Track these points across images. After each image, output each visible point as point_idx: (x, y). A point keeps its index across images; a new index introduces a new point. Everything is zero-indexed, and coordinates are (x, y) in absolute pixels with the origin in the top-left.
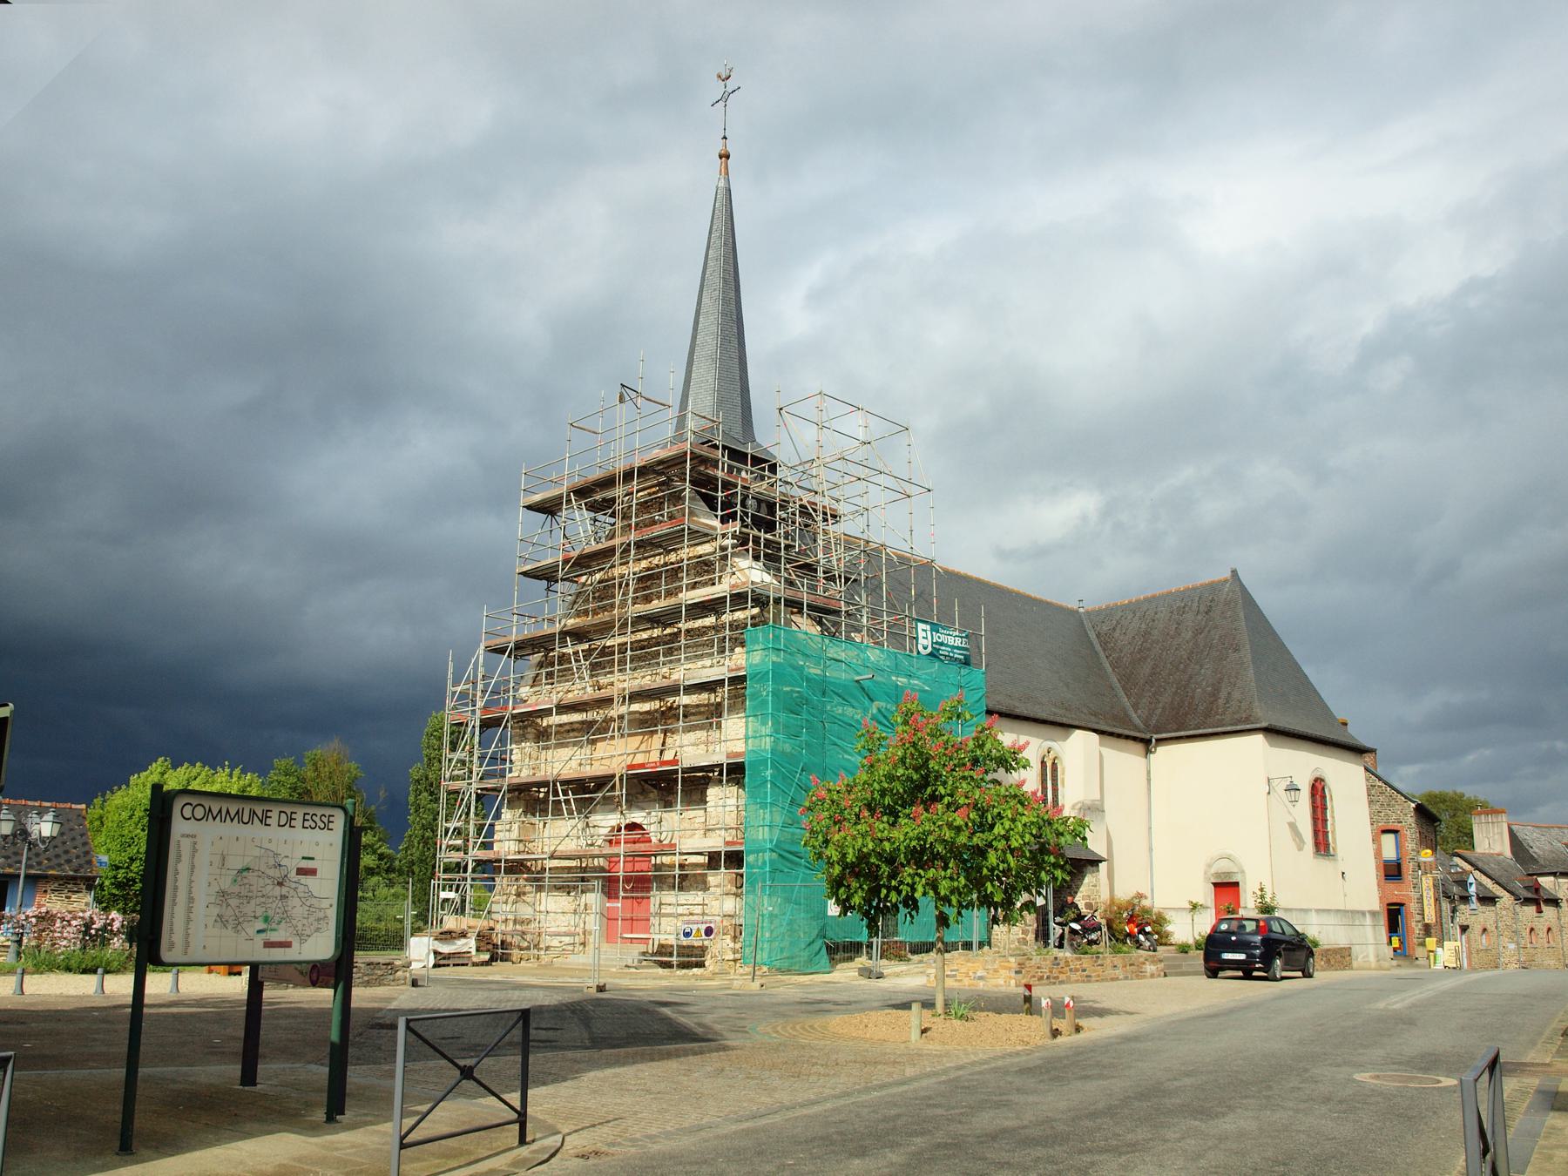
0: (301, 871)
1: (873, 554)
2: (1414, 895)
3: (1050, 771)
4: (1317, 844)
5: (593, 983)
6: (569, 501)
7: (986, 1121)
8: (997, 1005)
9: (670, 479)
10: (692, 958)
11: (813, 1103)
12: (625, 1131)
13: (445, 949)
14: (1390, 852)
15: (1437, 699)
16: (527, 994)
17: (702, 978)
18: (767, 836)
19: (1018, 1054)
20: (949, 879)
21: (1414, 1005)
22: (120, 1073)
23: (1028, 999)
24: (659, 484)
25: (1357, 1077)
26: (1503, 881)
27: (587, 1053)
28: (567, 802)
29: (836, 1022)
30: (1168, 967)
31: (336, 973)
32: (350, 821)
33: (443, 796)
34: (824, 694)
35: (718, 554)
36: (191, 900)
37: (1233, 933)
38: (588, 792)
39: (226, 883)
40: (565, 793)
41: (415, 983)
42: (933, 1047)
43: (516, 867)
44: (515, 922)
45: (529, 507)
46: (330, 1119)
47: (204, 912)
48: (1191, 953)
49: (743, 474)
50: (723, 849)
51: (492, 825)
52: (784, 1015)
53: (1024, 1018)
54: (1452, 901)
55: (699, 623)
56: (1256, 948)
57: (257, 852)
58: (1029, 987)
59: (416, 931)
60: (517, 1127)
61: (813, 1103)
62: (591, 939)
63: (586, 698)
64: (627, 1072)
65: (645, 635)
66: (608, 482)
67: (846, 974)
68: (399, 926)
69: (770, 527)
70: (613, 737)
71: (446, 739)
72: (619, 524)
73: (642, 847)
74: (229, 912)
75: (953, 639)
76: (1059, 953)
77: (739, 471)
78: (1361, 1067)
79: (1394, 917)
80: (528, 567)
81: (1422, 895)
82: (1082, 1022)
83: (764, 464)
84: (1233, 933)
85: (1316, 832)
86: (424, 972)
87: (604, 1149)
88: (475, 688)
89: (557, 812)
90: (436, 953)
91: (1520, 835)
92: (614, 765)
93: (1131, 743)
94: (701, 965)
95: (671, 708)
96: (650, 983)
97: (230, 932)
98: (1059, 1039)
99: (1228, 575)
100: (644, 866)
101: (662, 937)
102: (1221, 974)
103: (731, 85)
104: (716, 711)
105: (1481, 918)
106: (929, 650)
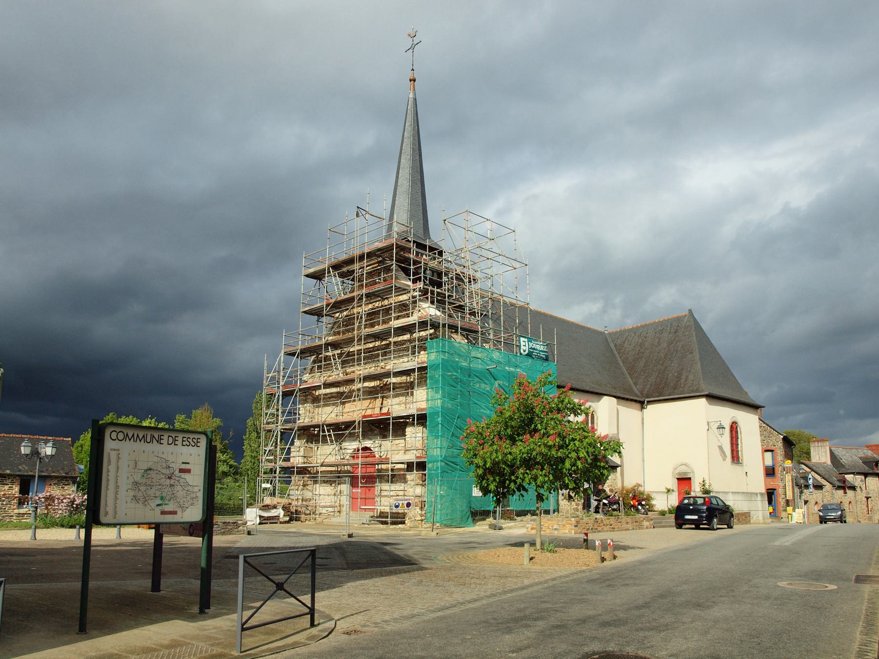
0: (181, 471)
2: (781, 484)
3: (591, 416)
4: (733, 457)
5: (346, 533)
6: (329, 272)
7: (576, 611)
8: (569, 544)
10: (398, 519)
11: (476, 600)
13: (266, 514)
14: (769, 462)
16: (310, 539)
17: (404, 530)
18: (439, 453)
19: (584, 571)
20: (543, 475)
21: (794, 544)
22: (78, 585)
23: (586, 541)
24: (379, 262)
25: (779, 584)
26: (826, 477)
27: (345, 572)
28: (330, 436)
29: (481, 553)
30: (655, 523)
31: (203, 528)
32: (210, 442)
33: (263, 434)
34: (469, 376)
35: (411, 300)
36: (117, 487)
37: (691, 505)
38: (341, 431)
39: (138, 477)
40: (329, 431)
41: (249, 533)
42: (536, 568)
43: (302, 471)
44: (303, 500)
45: (307, 276)
46: (202, 611)
47: (125, 493)
48: (667, 515)
50: (415, 460)
51: (289, 449)
52: (452, 550)
53: (584, 552)
54: (800, 487)
55: (401, 338)
56: (702, 512)
57: (156, 459)
58: (586, 534)
59: (250, 505)
61: (476, 600)
62: (344, 509)
63: (339, 379)
65: (371, 345)
66: (350, 261)
67: (482, 528)
68: (240, 502)
69: (439, 285)
70: (354, 401)
72: (357, 284)
73: (370, 460)
74: (140, 494)
76: (598, 516)
77: (422, 255)
79: (770, 495)
81: (786, 484)
82: (616, 553)
84: (691, 505)
85: (732, 451)
86: (254, 527)
87: (360, 628)
88: (279, 375)
89: (325, 441)
90: (260, 517)
91: (836, 453)
93: (633, 403)
94: (403, 523)
95: (386, 385)
96: (376, 533)
97: (140, 505)
98: (605, 563)
99: (687, 313)
100: (372, 470)
101: (382, 508)
102: (684, 527)
103: (416, 40)
104: (410, 386)
105: (815, 496)
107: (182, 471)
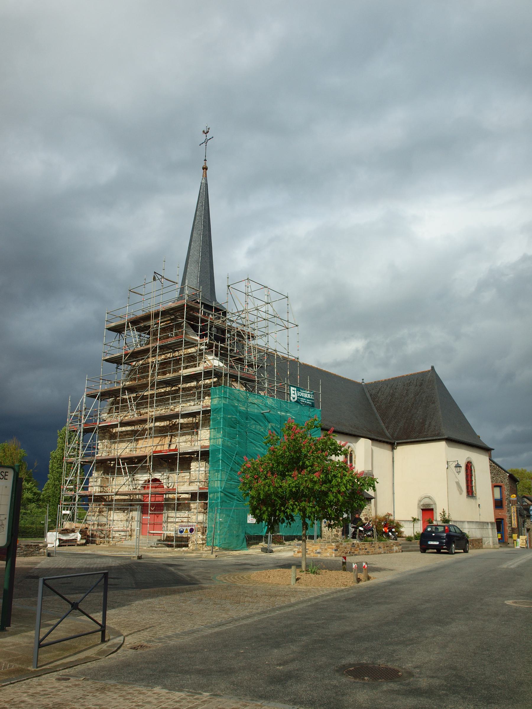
1: (270, 355)
2: (507, 515)
3: (349, 455)
6: (128, 327)
9: (176, 318)
12: (155, 634)
13: (64, 538)
14: (498, 496)
15: (509, 430)
16: (104, 560)
18: (219, 485)
21: (518, 567)
23: (344, 563)
24: (171, 320)
28: (124, 468)
29: (254, 574)
35: (198, 352)
36: (244, 559)
38: (135, 464)
40: (123, 464)
41: (49, 555)
42: (302, 587)
43: (99, 499)
44: (98, 525)
45: (109, 329)
48: (413, 541)
49: (210, 316)
50: (198, 491)
51: (88, 479)
52: (229, 571)
55: (188, 385)
58: (345, 558)
59: (51, 529)
60: (100, 633)
62: (135, 533)
63: (134, 419)
64: (154, 601)
66: (147, 318)
67: (255, 551)
68: (42, 526)
69: (223, 341)
70: (146, 438)
71: (66, 439)
73: (159, 490)
75: (306, 395)
76: (355, 541)
77: (209, 314)
78: (507, 597)
79: (499, 524)
80: (108, 357)
82: (371, 575)
83: (221, 312)
84: (433, 532)
85: (468, 486)
86: (53, 549)
87: (145, 644)
88: (81, 414)
89: (119, 473)
90: (60, 540)
92: (147, 451)
94: (187, 546)
95: (175, 424)
96: (162, 555)
98: (361, 583)
99: (430, 368)
100: (160, 499)
101: (168, 533)
103: (209, 136)
106: (296, 399)
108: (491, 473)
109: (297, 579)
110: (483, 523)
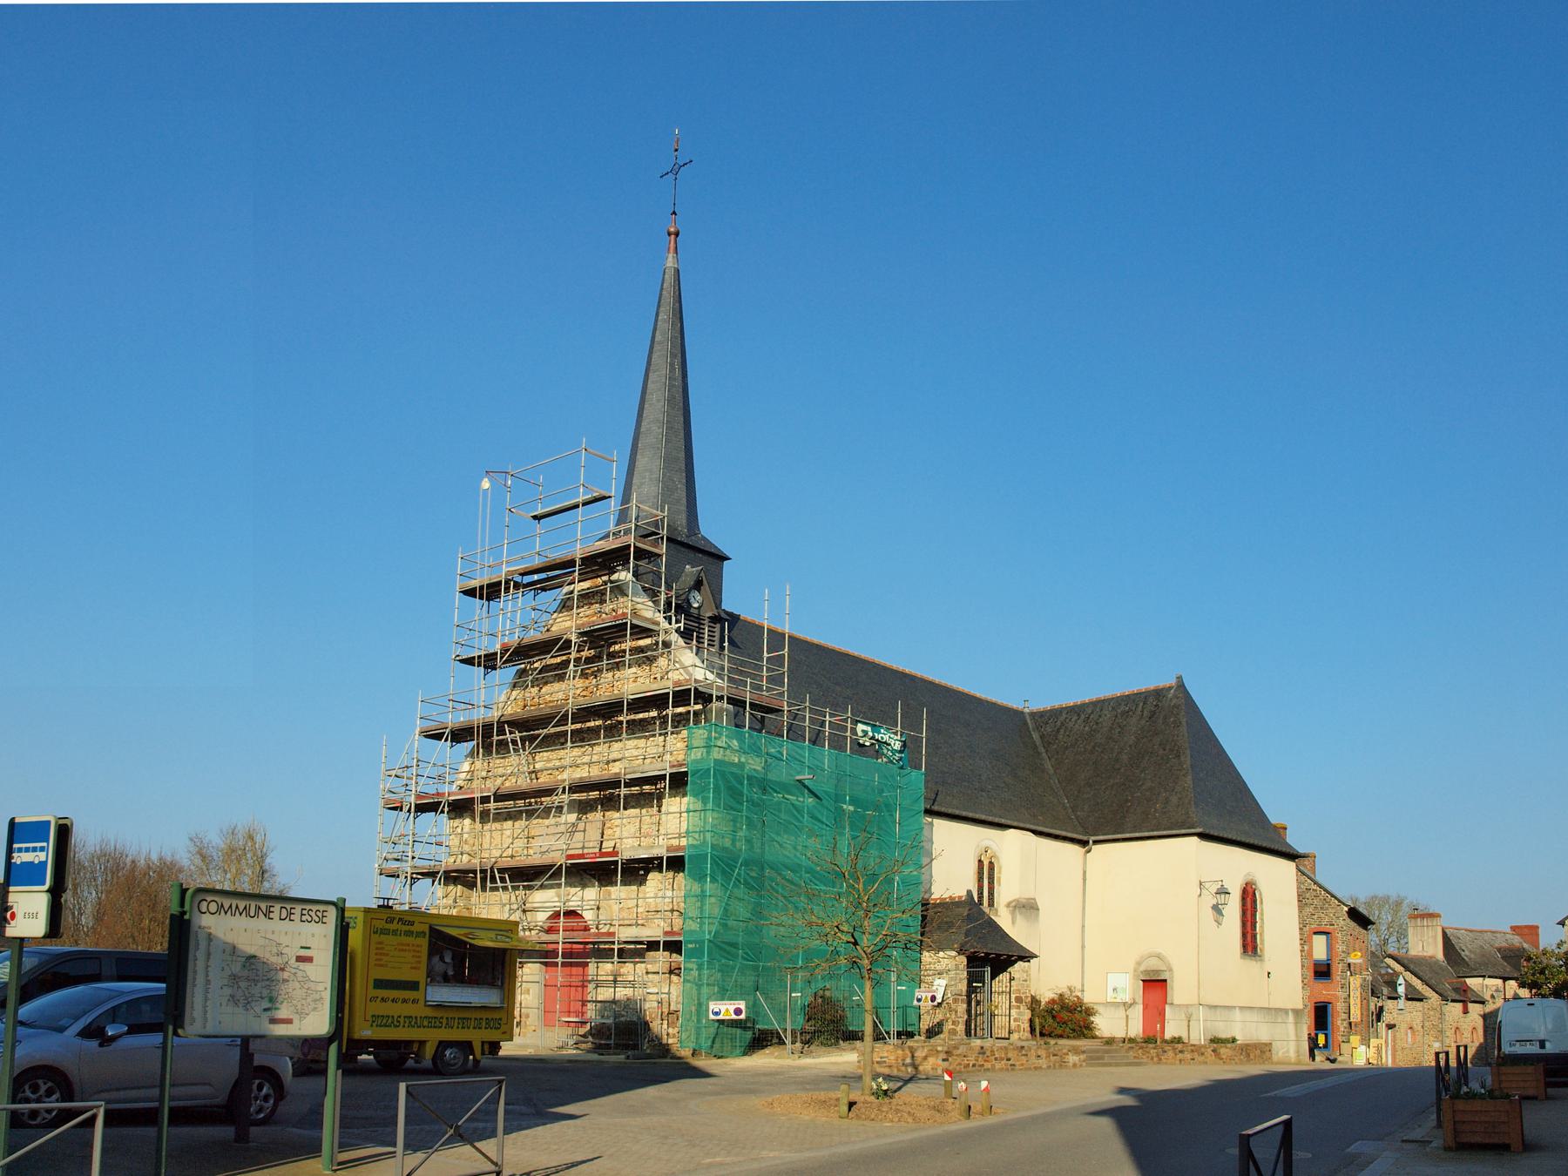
2: (1341, 994)
3: (986, 871)
4: (1245, 946)
14: (1320, 949)
36: (208, 982)
40: (503, 880)
57: (262, 941)
79: (1321, 1016)
97: (241, 1010)
107: (300, 959)
108: (1301, 908)
109: (851, 1105)
110: (1278, 1010)
